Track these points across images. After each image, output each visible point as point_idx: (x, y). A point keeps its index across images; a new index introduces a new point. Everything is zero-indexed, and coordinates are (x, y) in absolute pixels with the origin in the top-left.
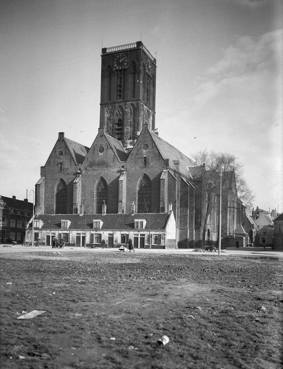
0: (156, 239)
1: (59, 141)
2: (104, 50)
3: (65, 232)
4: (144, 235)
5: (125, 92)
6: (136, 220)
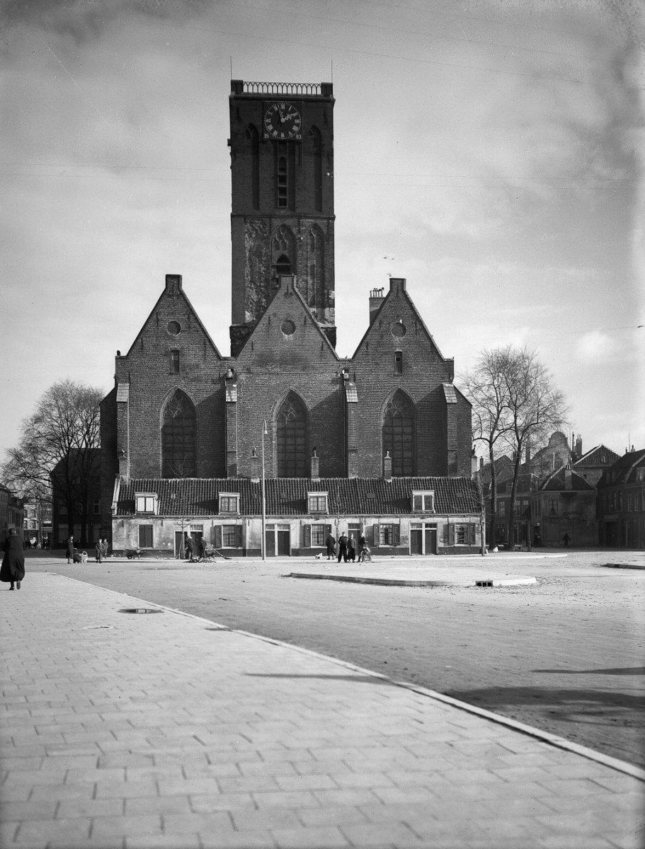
0: (462, 533)
1: (170, 296)
2: (237, 85)
3: (233, 522)
4: (435, 525)
5: (297, 195)
6: (416, 493)
